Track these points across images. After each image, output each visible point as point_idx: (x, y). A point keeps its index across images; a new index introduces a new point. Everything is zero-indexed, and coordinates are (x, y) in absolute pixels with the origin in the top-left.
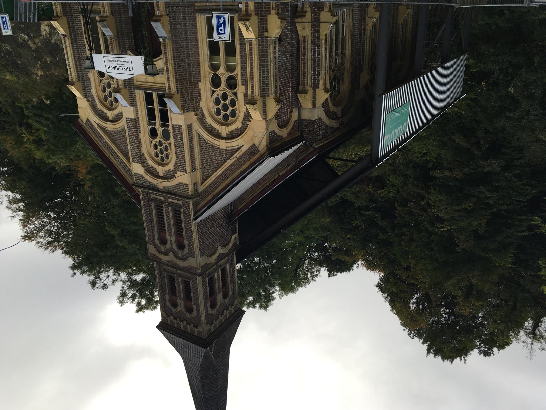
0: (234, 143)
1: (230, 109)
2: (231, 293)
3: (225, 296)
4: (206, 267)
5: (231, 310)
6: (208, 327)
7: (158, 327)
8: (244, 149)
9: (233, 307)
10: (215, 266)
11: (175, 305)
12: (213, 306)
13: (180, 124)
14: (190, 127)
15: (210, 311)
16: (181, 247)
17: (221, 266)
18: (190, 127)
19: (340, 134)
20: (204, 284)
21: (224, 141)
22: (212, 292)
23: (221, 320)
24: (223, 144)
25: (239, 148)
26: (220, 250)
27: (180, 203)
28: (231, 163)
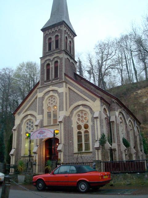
0: (25, 114)
1: (81, 119)
2: (47, 39)
3: (50, 39)
4: (60, 52)
5: (54, 30)
6: (61, 28)
7: (76, 35)
8: (22, 113)
9: (47, 33)
10: (54, 52)
11: (70, 41)
12: (57, 36)
13: (38, 116)
15: (59, 34)
17: (51, 51)
19: (11, 164)
21: (28, 114)
23: (57, 28)
24: (28, 113)
25: (24, 112)
27: (45, 84)
28: (75, 90)
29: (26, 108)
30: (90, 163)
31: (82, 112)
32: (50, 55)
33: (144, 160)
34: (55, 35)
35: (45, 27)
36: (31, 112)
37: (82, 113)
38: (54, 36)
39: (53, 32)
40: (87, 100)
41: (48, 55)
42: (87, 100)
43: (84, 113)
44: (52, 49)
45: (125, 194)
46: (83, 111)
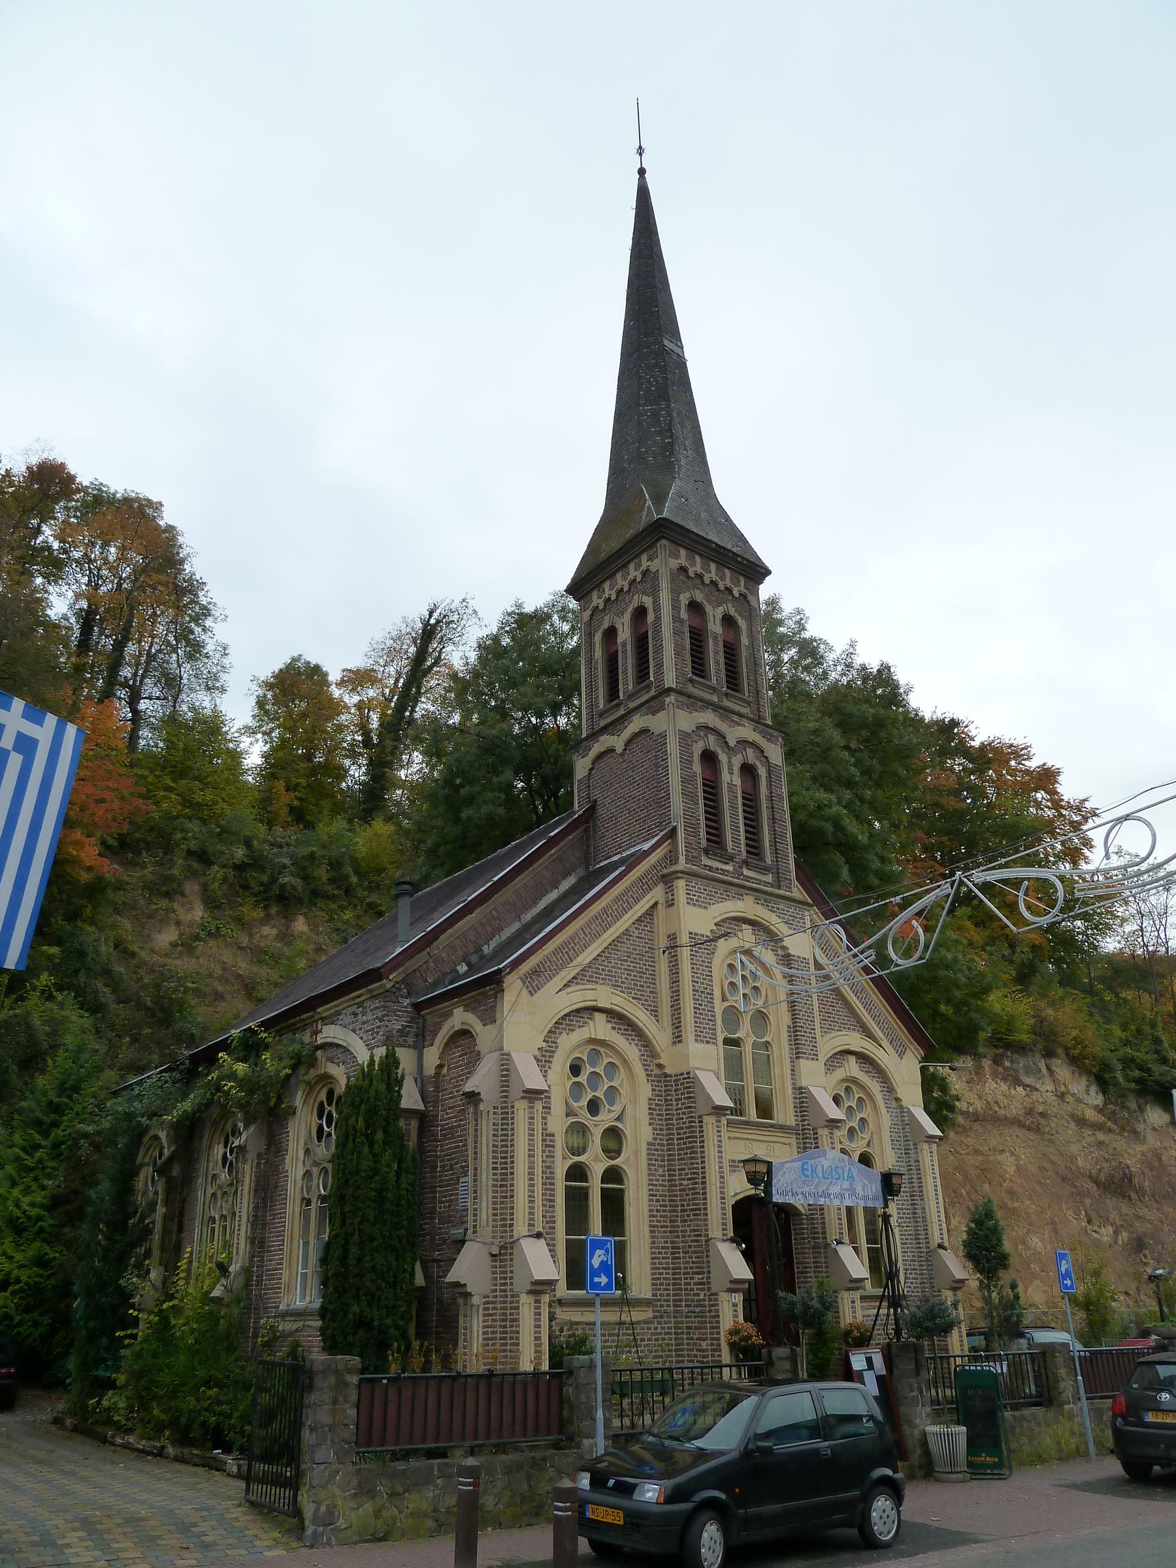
4: (654, 705)
5: (636, 570)
6: (654, 565)
8: (558, 981)
10: (632, 705)
11: (728, 620)
12: (640, 612)
14: (678, 1038)
15: (648, 601)
16: (709, 758)
18: (678, 1038)
20: (659, 666)
21: (601, 1004)
22: (641, 643)
24: (605, 996)
26: (617, 742)
29: (585, 958)
30: (712, 1367)
31: (597, 1052)
32: (612, 727)
33: (721, 1367)
34: (630, 609)
35: (684, 458)
36: (590, 995)
37: (595, 1055)
38: (627, 616)
39: (608, 600)
40: (876, 1041)
41: (604, 730)
42: (876, 1041)
43: (606, 1060)
44: (621, 695)
45: (412, 1143)
46: (602, 1050)
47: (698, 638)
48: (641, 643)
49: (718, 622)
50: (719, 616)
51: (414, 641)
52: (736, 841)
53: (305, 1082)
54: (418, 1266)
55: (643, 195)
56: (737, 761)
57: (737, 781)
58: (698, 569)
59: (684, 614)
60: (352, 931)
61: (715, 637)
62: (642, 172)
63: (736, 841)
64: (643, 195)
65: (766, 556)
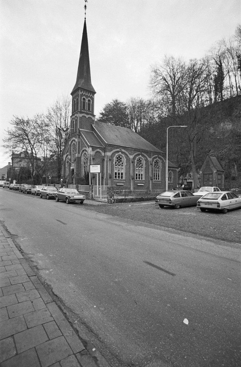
11: (89, 101)
12: (77, 99)
22: (77, 103)
47: (84, 103)
48: (77, 103)
49: (87, 101)
50: (88, 100)
51: (59, 132)
52: (87, 108)
53: (78, 190)
54: (34, 175)
55: (85, 21)
56: (88, 99)
57: (87, 102)
58: (87, 94)
59: (82, 100)
60: (30, 136)
61: (87, 103)
62: (85, 18)
63: (87, 108)
64: (85, 21)
65: (96, 91)
